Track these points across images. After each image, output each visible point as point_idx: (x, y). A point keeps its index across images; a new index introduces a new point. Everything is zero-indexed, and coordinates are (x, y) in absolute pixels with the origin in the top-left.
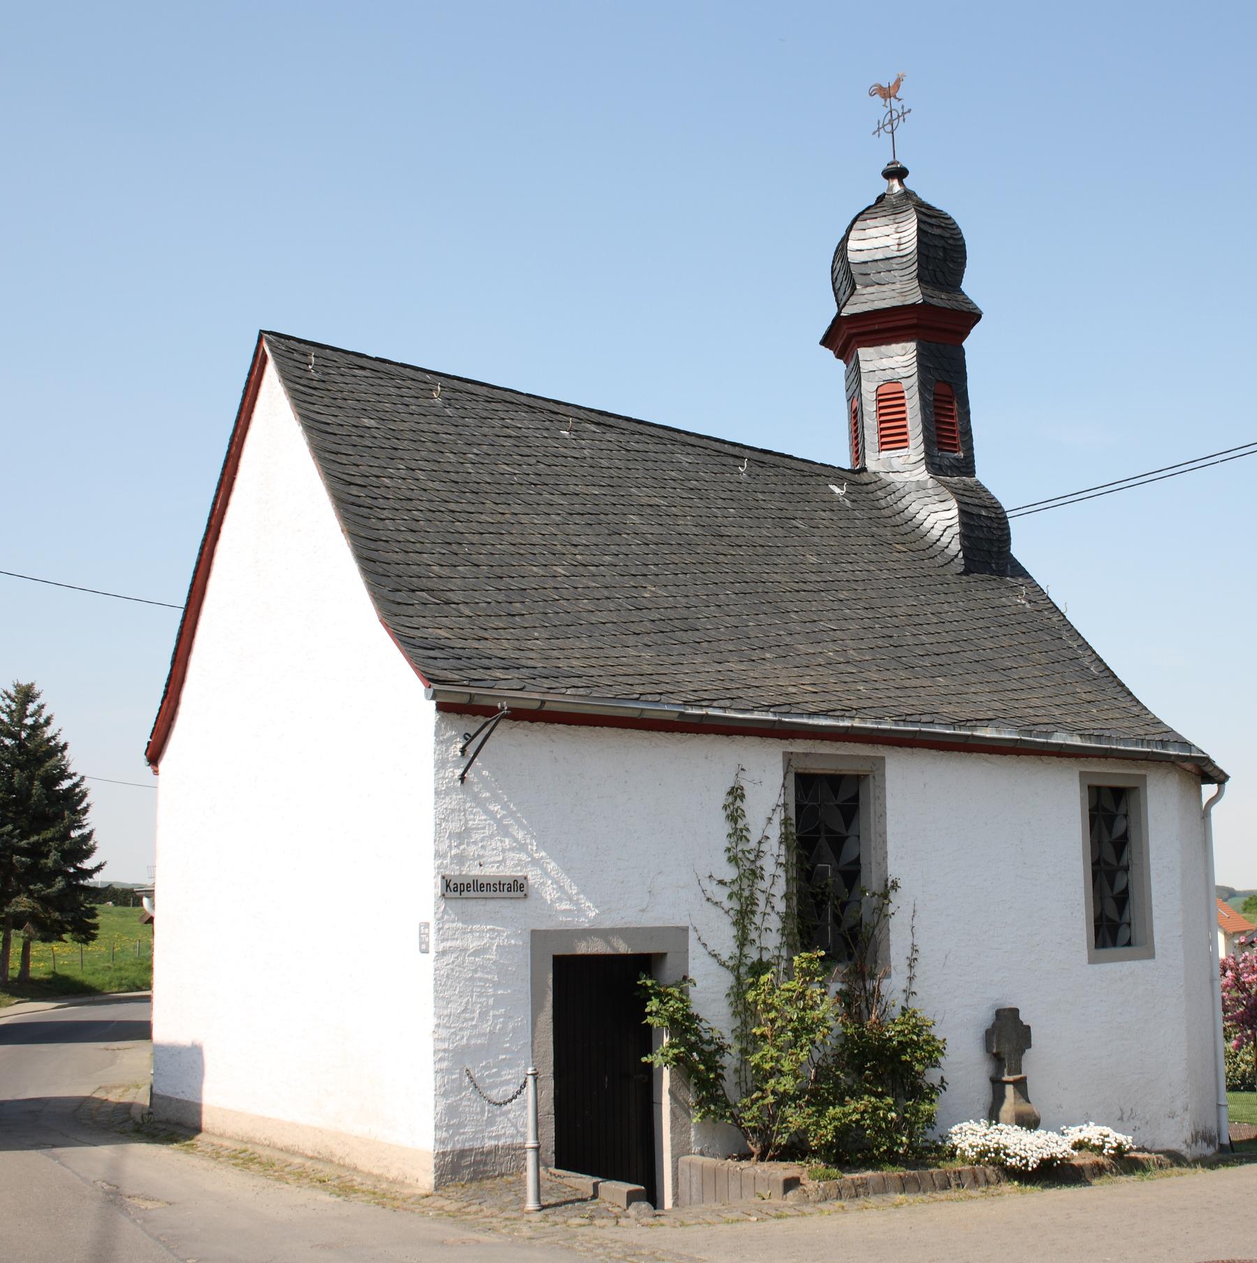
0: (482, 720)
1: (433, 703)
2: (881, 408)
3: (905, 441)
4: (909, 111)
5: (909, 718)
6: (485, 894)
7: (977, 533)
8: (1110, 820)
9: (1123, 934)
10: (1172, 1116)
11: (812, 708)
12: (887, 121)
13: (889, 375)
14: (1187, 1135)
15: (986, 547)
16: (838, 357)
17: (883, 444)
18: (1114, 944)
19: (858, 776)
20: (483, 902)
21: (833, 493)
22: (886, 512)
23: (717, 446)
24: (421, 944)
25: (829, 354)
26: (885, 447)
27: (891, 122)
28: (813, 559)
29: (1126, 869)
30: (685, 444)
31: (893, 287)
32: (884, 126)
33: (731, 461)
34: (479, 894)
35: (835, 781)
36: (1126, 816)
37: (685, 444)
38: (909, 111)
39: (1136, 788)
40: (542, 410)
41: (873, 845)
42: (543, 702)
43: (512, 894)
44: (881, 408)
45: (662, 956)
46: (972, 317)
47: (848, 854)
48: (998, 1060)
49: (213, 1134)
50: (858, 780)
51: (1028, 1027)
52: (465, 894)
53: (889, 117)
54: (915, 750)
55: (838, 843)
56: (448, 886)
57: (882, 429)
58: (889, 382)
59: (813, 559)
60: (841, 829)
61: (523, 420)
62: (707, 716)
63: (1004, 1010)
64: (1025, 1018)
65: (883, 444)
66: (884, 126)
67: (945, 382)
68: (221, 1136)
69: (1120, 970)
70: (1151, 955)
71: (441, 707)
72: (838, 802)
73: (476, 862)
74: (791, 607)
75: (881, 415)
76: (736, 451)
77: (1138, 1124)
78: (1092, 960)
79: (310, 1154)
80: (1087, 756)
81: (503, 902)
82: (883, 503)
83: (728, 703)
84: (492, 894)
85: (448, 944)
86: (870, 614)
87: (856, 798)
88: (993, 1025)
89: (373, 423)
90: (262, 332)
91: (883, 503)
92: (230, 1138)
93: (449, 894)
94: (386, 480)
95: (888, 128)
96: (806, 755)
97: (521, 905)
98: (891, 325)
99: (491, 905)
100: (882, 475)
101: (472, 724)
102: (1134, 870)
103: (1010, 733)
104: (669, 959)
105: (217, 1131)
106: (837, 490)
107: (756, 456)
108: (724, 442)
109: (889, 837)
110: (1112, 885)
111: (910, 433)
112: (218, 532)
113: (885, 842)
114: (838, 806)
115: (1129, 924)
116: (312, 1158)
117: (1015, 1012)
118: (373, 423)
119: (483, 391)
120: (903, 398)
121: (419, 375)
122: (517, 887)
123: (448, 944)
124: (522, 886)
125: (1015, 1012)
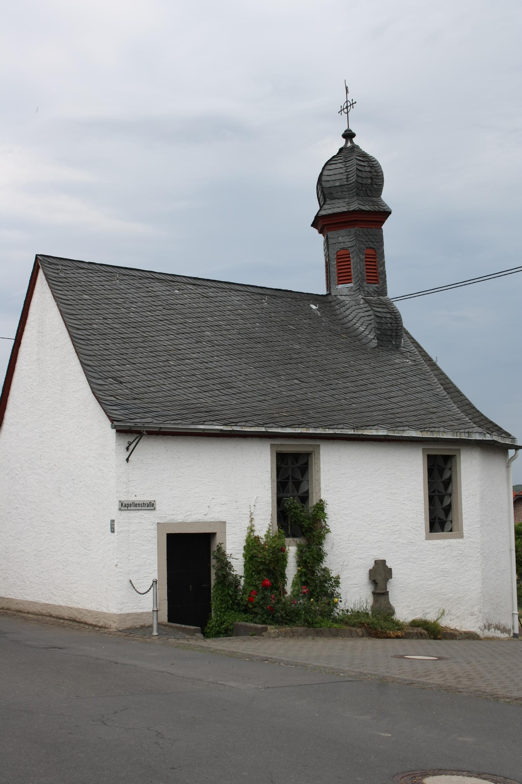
0: (135, 436)
1: (115, 430)
2: (338, 262)
3: (350, 279)
4: (355, 103)
5: (331, 427)
6: (137, 508)
7: (385, 327)
8: (441, 472)
9: (448, 526)
10: (472, 614)
11: (283, 424)
12: (345, 107)
13: (342, 245)
14: (481, 624)
15: (389, 333)
16: (320, 233)
17: (339, 281)
18: (443, 531)
19: (308, 453)
20: (137, 511)
21: (312, 309)
22: (340, 317)
23: (252, 290)
24: (111, 529)
25: (316, 231)
26: (340, 282)
27: (347, 107)
28: (297, 347)
29: (450, 495)
30: (236, 290)
31: (344, 200)
32: (343, 109)
33: (259, 297)
34: (135, 508)
35: (296, 456)
36: (450, 469)
37: (236, 290)
38: (355, 103)
39: (454, 456)
40: (166, 281)
41: (314, 485)
42: (161, 428)
43: (149, 508)
44: (338, 262)
45: (214, 534)
46: (387, 213)
47: (303, 489)
48: (374, 582)
49: (24, 612)
50: (308, 455)
51: (391, 569)
52: (129, 508)
53: (346, 105)
54: (335, 441)
55: (297, 484)
56: (122, 505)
57: (339, 273)
58: (343, 249)
59: (297, 347)
60: (300, 478)
61: (158, 287)
62: (233, 431)
63: (378, 561)
64: (389, 564)
65: (339, 281)
66: (343, 109)
67: (371, 248)
68: (28, 613)
69: (442, 543)
70: (462, 537)
71: (117, 431)
72: (298, 465)
73: (134, 495)
74: (281, 373)
75: (339, 266)
76: (260, 291)
77: (452, 617)
78: (427, 538)
79: (67, 618)
80: (427, 441)
81: (145, 512)
82: (338, 312)
83: (244, 424)
84: (140, 508)
85: (122, 529)
86: (323, 373)
87: (307, 463)
88: (373, 568)
89: (88, 297)
90: (37, 255)
91: (338, 312)
92: (32, 614)
93: (122, 508)
94: (94, 325)
95: (346, 110)
96: (282, 445)
97: (153, 512)
98: (343, 220)
99: (140, 513)
100: (339, 297)
101: (131, 438)
102: (454, 495)
103: (383, 432)
104: (218, 536)
105: (26, 611)
106: (313, 307)
107: (272, 293)
108: (256, 287)
109: (322, 481)
110: (442, 502)
111: (353, 275)
112: (20, 343)
113: (320, 483)
114: (298, 467)
115: (451, 521)
116: (67, 620)
117: (384, 562)
118: (88, 297)
119: (138, 273)
120: (349, 257)
121: (109, 269)
122: (150, 506)
123: (122, 529)
124: (153, 504)
125: (384, 562)
